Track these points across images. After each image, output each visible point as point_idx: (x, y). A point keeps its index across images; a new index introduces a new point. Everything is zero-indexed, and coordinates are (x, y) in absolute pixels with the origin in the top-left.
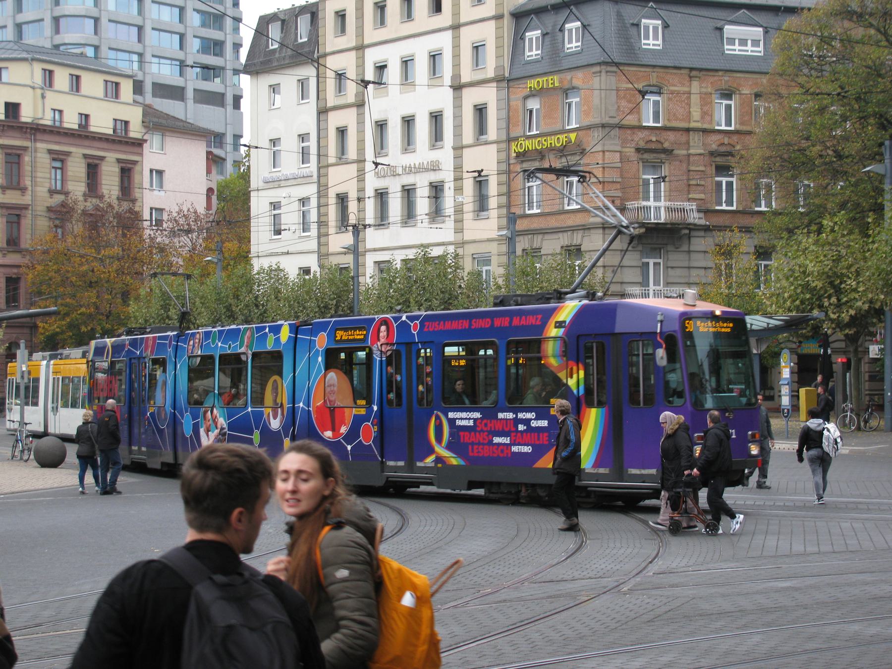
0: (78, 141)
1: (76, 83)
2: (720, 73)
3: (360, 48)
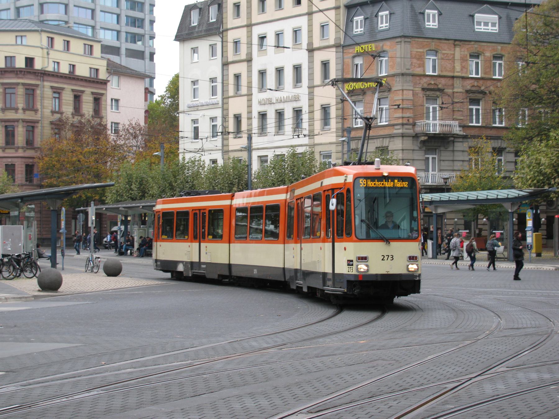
0: (68, 81)
2: (473, 43)
3: (249, 26)
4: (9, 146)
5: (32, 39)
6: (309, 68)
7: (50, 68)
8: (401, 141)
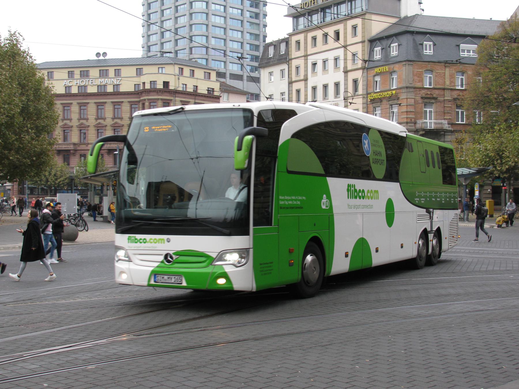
3: (306, 56)
5: (169, 69)
7: (180, 89)
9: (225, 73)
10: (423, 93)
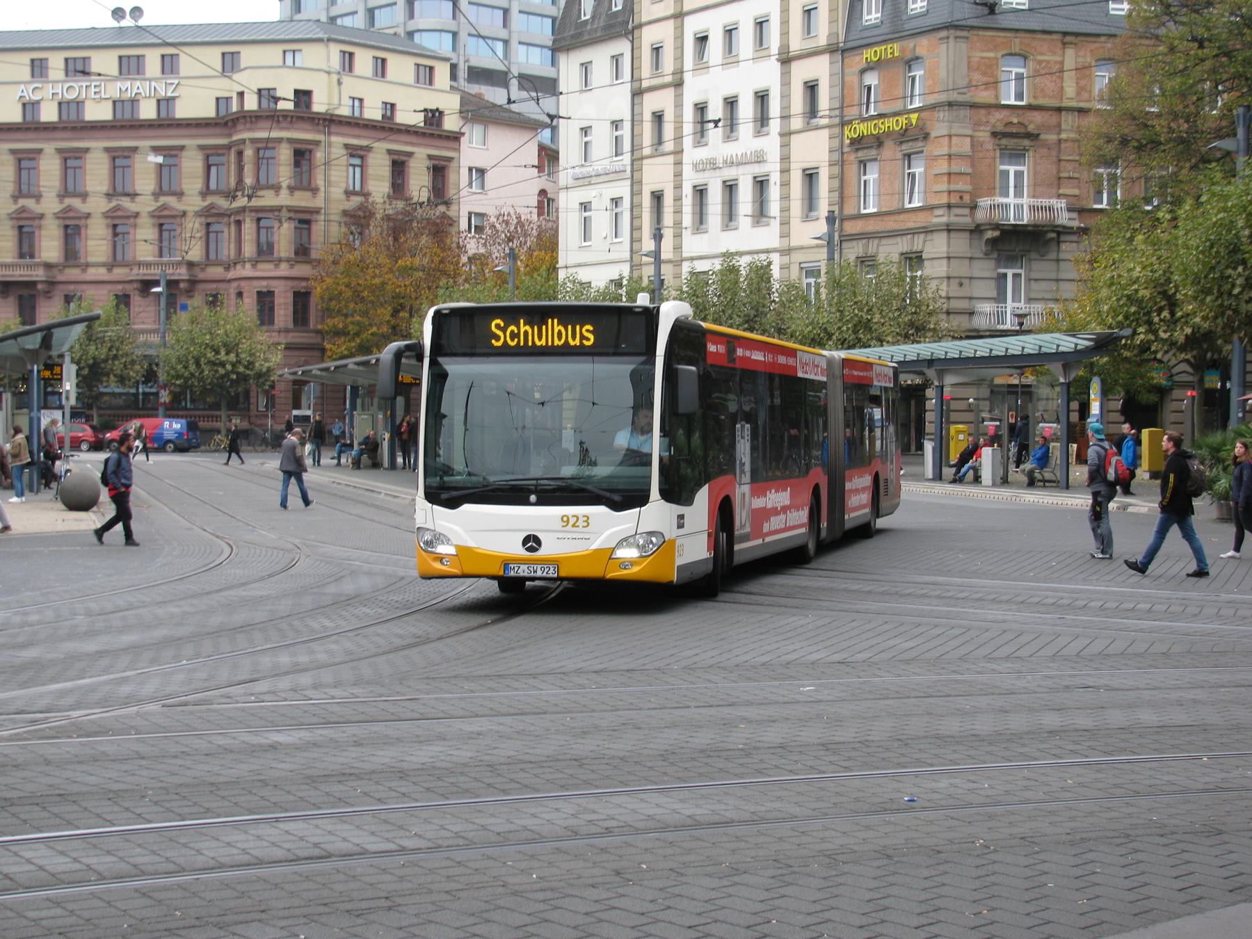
1: (381, 67)
2: (1103, 39)
3: (679, 16)
4: (263, 258)
5: (313, 56)
6: (782, 97)
7: (345, 111)
8: (945, 241)
9: (506, 74)
10: (998, 117)
